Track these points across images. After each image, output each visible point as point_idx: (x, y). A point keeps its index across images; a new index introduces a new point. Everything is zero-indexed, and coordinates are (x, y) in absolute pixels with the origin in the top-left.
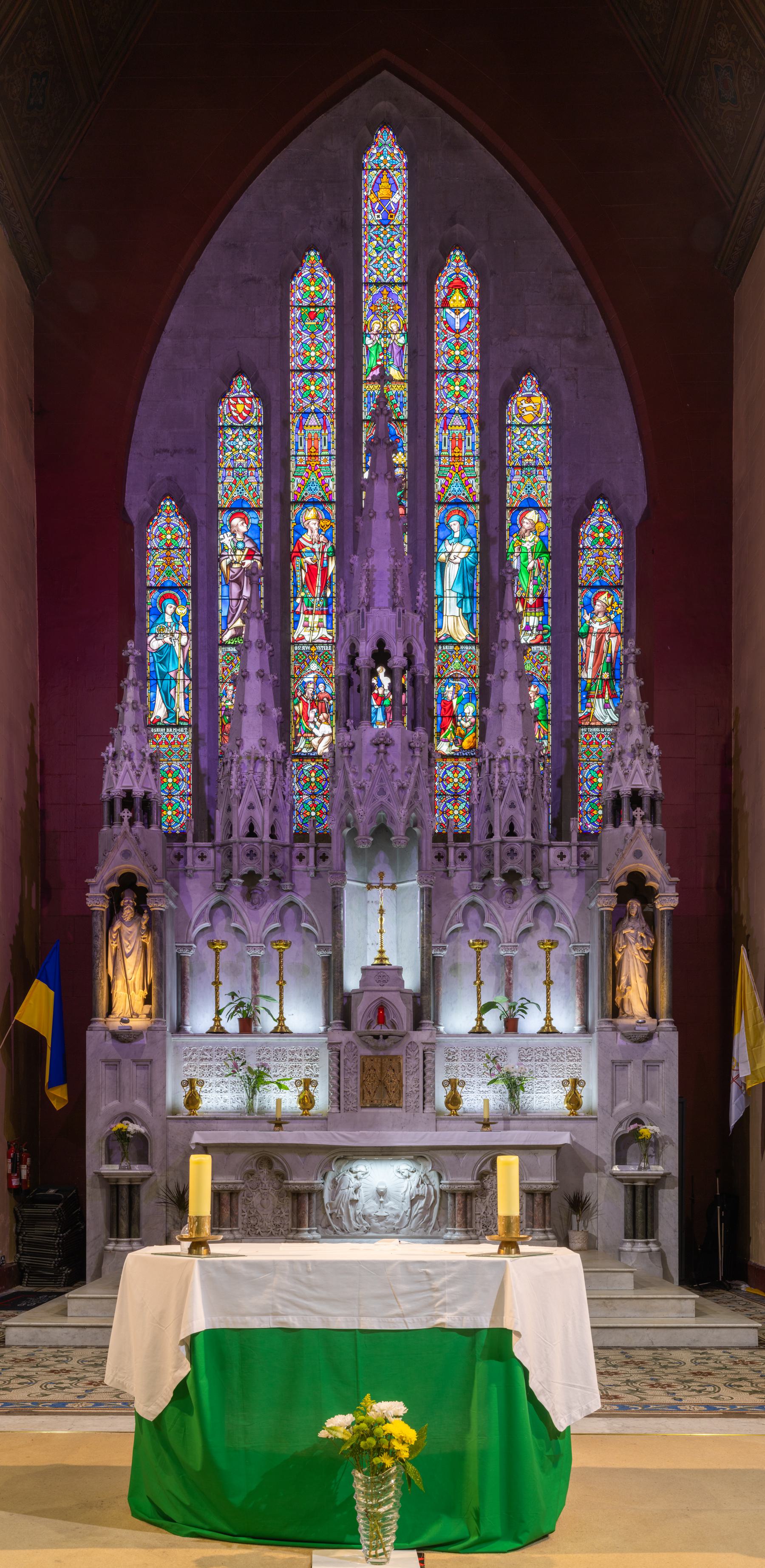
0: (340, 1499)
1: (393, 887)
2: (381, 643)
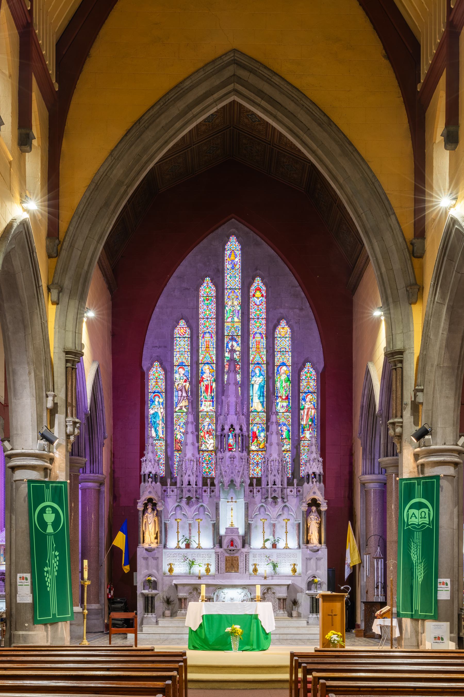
0: (229, 643)
1: (236, 502)
2: (232, 426)
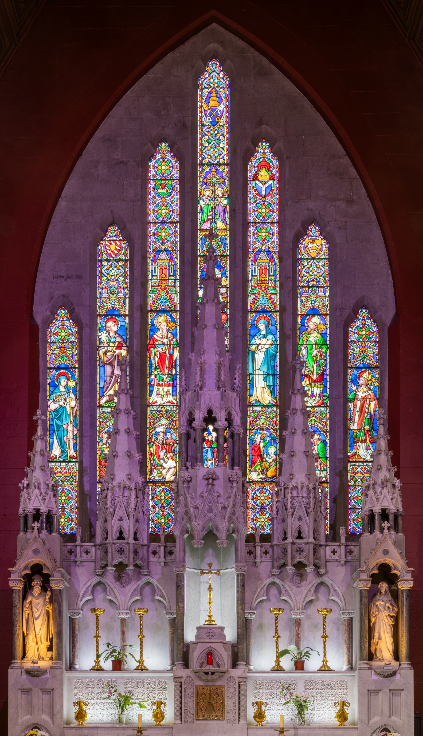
1: (218, 573)
2: (210, 412)
